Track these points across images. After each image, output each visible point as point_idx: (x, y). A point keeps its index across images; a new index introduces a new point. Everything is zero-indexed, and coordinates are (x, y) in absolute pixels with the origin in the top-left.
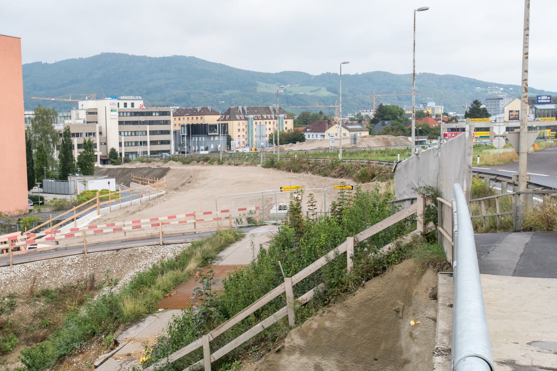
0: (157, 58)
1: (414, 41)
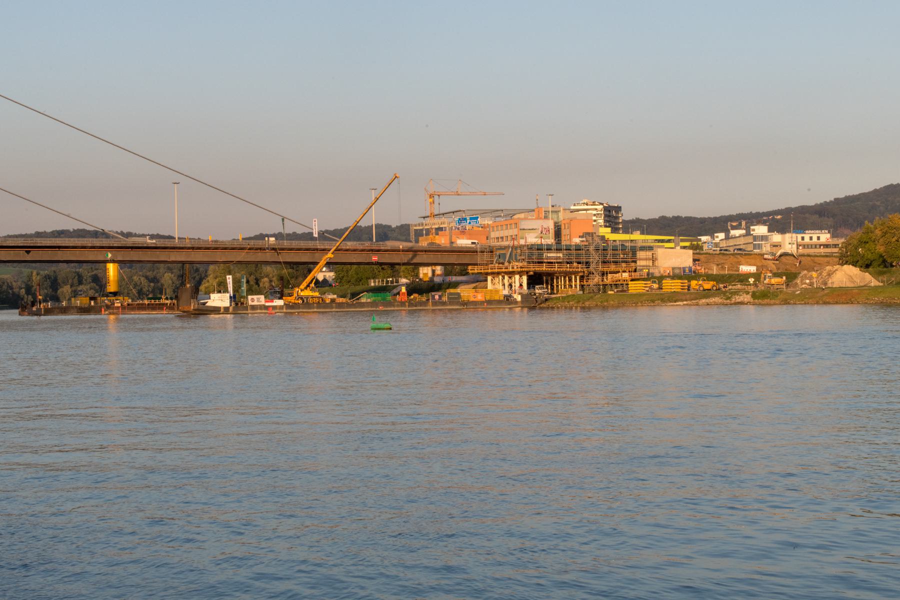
0: (783, 210)
1: (283, 224)
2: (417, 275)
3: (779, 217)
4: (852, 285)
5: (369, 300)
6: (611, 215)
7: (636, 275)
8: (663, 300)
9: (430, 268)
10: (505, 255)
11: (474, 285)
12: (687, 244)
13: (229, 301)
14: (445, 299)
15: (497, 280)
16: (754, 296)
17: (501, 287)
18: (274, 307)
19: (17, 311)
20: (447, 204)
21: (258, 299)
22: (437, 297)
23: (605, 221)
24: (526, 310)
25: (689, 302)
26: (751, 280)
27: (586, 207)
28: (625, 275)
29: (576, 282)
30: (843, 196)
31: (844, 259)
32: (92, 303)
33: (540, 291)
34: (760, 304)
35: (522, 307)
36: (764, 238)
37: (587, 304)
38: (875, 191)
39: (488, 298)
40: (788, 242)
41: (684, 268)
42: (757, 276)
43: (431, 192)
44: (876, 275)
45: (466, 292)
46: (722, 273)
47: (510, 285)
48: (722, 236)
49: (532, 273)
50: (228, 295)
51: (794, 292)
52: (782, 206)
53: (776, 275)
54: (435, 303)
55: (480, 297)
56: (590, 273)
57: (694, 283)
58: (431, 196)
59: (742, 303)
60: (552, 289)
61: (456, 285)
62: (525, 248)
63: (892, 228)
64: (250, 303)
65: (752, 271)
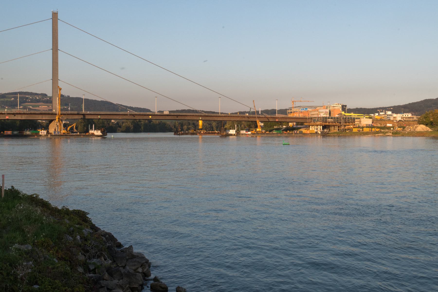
2: (288, 125)
3: (392, 108)
4: (423, 131)
5: (276, 133)
6: (344, 108)
7: (354, 126)
8: (364, 134)
9: (292, 123)
10: (315, 120)
11: (306, 128)
12: (368, 117)
13: (235, 132)
14: (298, 132)
15: (313, 127)
16: (393, 133)
17: (314, 129)
18: (248, 134)
19: (173, 133)
20: (297, 104)
21: (244, 132)
22: (296, 132)
23: (342, 110)
24: (322, 136)
25: (372, 135)
26: (392, 129)
27: (336, 105)
28: (352, 126)
29: (337, 128)
30: (411, 102)
31: (420, 122)
32: (195, 132)
33: (326, 131)
34: (395, 136)
35: (321, 135)
36: (390, 115)
37: (340, 135)
38: (421, 101)
39: (311, 132)
40: (399, 117)
41: (370, 125)
42: (393, 127)
43: (293, 101)
44: (431, 128)
45: (304, 131)
46: (381, 126)
47: (317, 129)
48: (377, 114)
49: (323, 125)
50: (235, 130)
51: (405, 132)
52: (393, 105)
53: (399, 127)
54: (295, 134)
55: (308, 132)
56: (341, 125)
57: (373, 129)
58: (293, 102)
59: (389, 136)
60: (329, 130)
61: (300, 128)
62: (322, 118)
63: (436, 114)
64: (241, 133)
65: (391, 126)
